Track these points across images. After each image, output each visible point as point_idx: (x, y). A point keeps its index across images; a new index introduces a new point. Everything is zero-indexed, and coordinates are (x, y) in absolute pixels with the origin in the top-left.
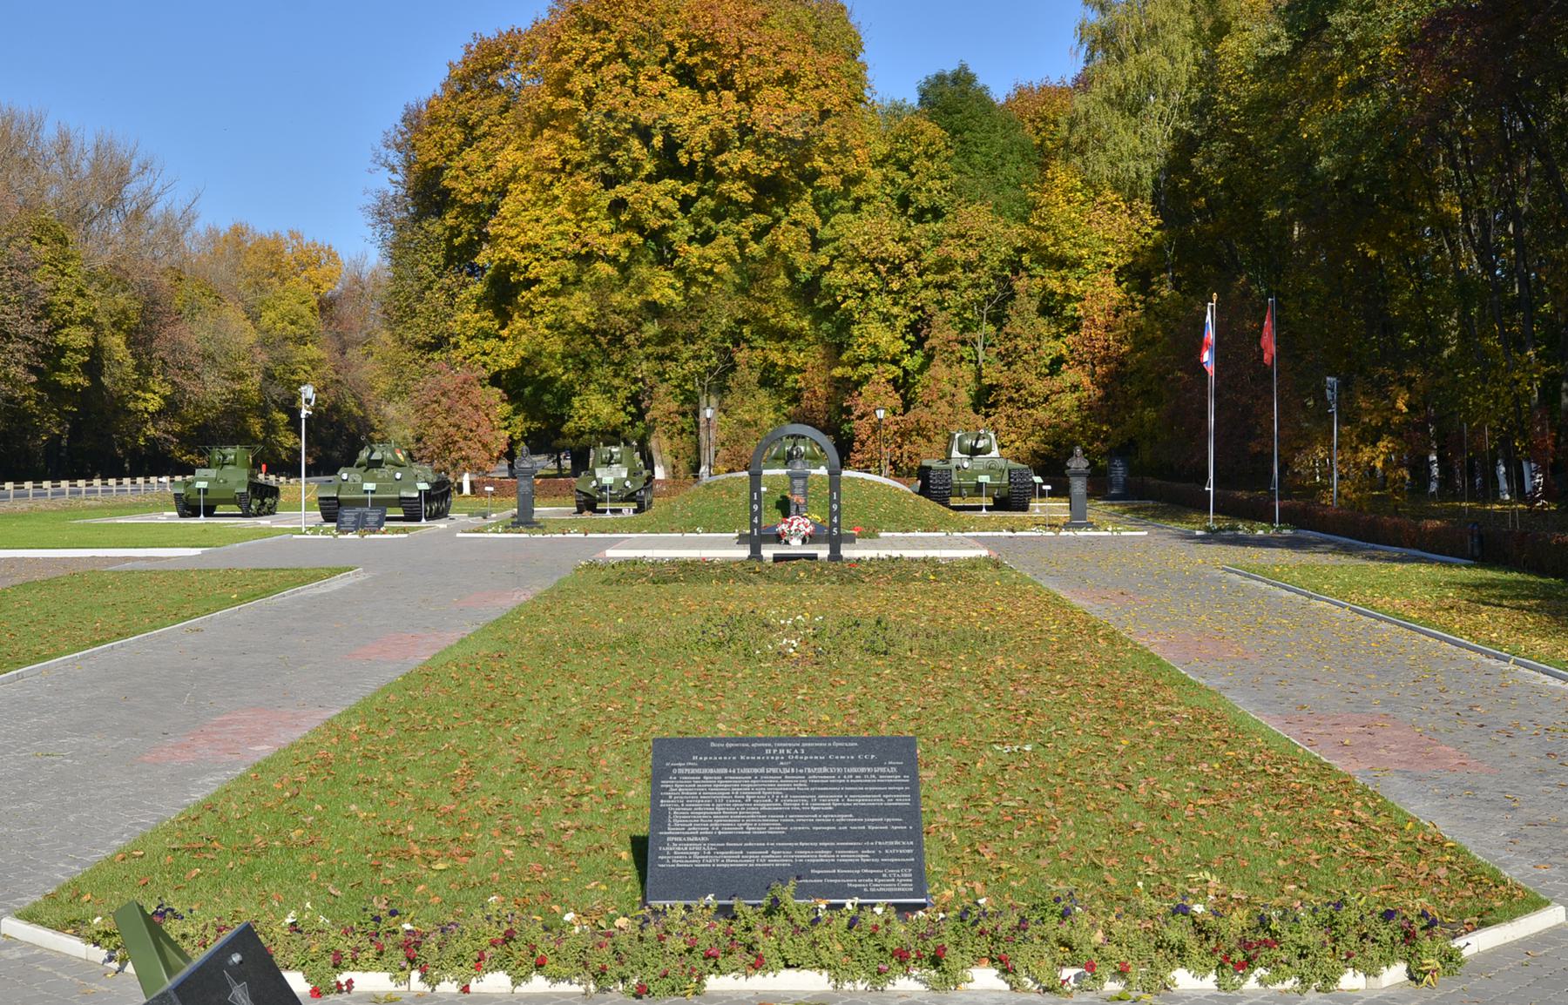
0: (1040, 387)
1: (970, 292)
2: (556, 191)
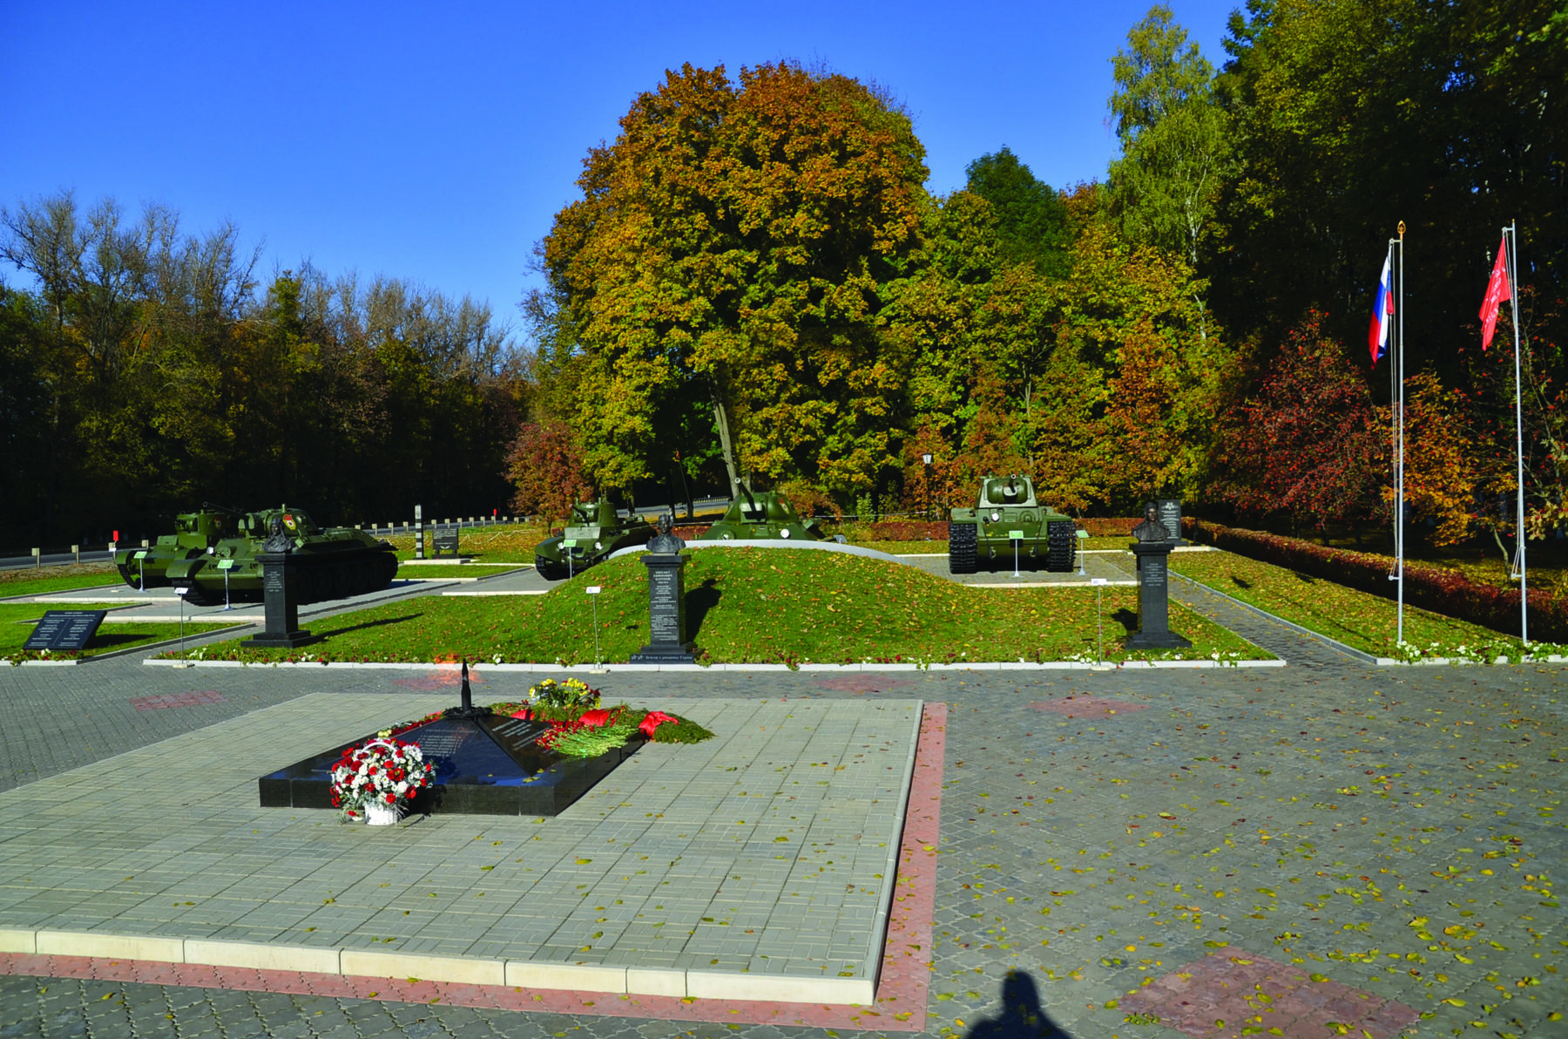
0: (1083, 429)
2: (638, 268)
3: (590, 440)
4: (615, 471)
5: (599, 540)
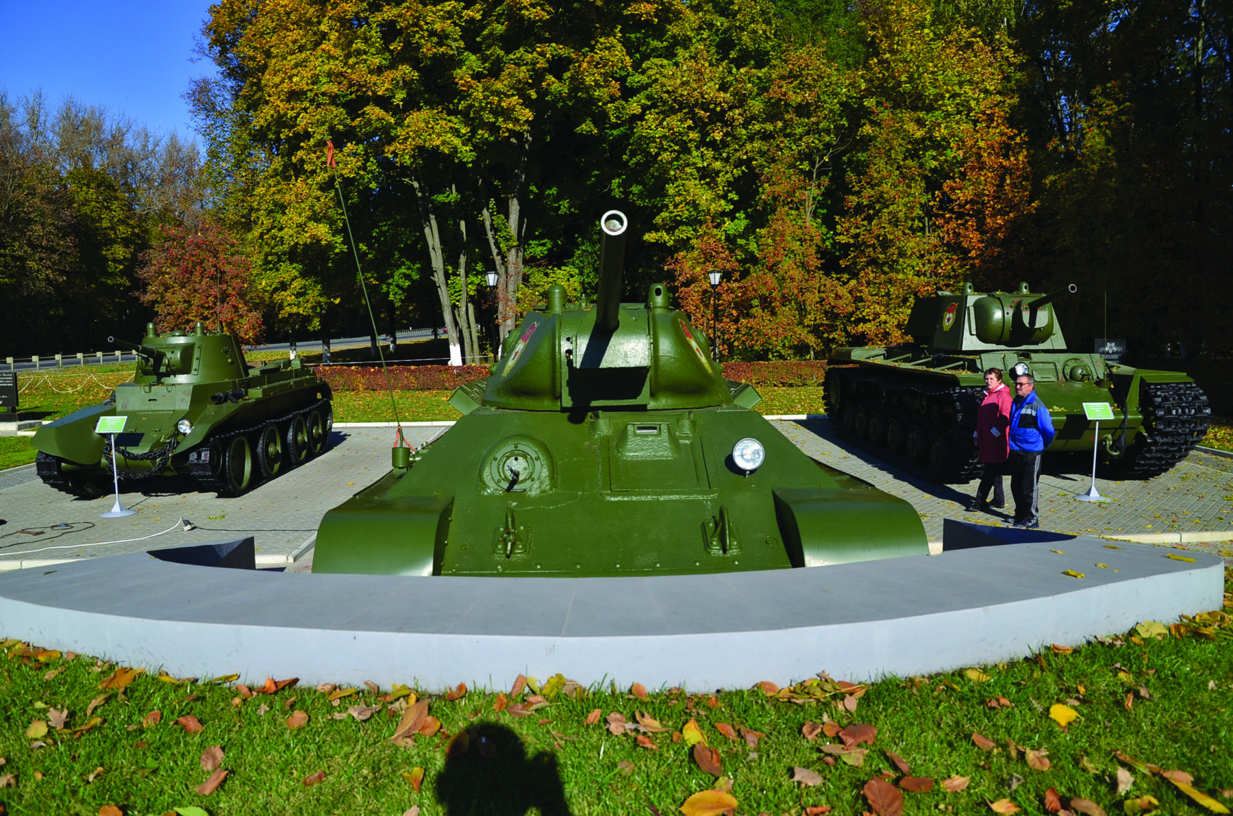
1: (810, 139)
2: (324, 28)
4: (298, 295)
5: (189, 416)
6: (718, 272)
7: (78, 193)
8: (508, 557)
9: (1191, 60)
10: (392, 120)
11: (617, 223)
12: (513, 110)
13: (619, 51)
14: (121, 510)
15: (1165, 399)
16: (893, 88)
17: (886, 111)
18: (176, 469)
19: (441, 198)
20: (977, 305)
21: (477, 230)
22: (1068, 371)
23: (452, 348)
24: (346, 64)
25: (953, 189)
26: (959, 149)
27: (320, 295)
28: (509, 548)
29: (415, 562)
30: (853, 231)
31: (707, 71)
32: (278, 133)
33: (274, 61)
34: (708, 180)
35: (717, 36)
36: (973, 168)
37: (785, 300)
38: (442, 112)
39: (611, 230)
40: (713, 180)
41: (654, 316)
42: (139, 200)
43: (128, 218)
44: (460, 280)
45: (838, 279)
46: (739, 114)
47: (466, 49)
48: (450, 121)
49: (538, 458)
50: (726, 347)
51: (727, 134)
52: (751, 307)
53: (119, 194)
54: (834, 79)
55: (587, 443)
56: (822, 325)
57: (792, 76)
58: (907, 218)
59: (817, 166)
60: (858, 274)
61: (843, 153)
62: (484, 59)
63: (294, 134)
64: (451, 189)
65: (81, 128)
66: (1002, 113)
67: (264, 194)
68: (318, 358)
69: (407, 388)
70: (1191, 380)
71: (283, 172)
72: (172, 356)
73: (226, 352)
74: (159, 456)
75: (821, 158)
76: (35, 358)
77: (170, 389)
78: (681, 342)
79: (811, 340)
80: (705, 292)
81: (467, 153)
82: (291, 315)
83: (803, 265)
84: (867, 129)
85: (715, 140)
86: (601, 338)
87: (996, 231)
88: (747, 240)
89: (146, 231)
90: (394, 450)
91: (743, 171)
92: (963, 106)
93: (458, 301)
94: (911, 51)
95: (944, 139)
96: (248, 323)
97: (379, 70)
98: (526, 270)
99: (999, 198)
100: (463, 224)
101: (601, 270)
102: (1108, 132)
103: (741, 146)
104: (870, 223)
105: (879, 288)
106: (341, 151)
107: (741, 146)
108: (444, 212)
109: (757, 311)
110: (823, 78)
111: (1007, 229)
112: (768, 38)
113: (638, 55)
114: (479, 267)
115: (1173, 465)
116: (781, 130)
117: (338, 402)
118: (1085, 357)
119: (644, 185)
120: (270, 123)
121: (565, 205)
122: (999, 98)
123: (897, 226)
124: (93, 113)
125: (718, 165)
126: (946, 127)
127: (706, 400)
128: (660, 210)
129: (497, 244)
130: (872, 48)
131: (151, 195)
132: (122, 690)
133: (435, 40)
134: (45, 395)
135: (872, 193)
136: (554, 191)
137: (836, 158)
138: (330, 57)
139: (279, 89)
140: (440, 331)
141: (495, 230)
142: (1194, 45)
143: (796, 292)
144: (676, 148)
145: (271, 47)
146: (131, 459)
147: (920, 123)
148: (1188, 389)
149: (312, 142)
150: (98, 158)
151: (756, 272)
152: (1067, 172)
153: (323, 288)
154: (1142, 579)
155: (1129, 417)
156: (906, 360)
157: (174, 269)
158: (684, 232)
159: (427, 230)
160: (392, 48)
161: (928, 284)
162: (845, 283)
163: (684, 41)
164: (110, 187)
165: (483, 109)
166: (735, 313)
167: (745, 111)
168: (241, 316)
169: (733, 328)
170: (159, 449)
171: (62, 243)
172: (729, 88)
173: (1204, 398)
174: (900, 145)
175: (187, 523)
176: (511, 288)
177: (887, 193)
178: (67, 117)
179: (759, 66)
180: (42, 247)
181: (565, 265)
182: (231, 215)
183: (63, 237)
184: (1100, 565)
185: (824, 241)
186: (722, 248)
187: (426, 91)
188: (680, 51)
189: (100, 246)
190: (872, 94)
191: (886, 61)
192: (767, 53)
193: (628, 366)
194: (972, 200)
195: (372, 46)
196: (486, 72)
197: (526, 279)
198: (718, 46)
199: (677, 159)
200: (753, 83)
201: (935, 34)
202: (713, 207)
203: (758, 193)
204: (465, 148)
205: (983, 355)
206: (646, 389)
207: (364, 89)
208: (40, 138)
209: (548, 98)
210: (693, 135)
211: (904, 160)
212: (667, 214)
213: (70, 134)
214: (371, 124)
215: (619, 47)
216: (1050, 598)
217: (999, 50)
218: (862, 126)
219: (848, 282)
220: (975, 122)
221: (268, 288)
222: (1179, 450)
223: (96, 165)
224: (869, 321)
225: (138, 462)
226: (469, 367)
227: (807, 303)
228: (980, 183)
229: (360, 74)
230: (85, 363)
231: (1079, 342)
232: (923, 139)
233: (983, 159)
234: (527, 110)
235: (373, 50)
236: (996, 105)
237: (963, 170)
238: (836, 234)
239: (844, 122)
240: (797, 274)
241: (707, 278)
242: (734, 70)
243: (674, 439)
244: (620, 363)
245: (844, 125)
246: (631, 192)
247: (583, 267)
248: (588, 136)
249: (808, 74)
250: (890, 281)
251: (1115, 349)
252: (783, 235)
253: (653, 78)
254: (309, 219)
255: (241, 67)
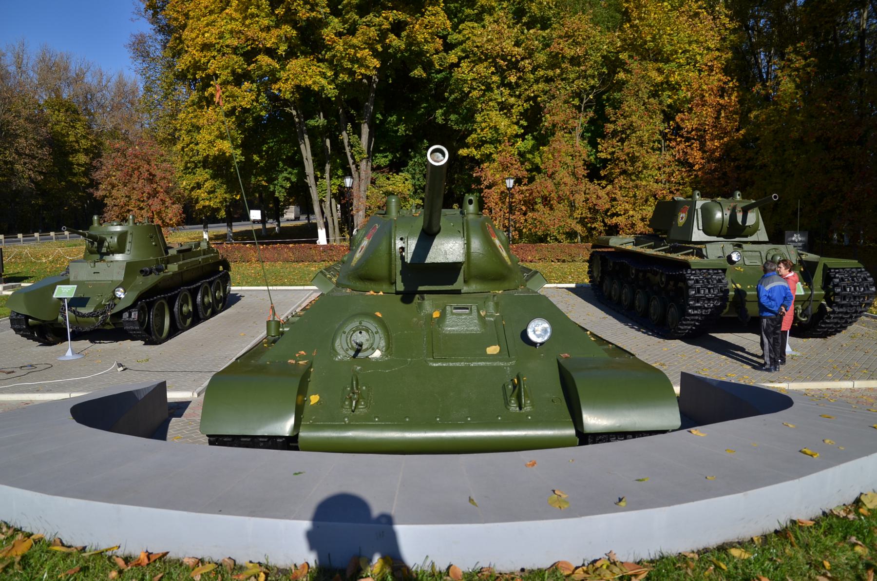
1: (580, 82)
3: (189, 165)
4: (209, 193)
5: (123, 285)
6: (512, 178)
7: (52, 116)
8: (353, 411)
9: (858, 27)
10: (277, 66)
11: (440, 155)
12: (365, 59)
13: (442, 17)
14: (73, 354)
15: (842, 280)
16: (641, 46)
17: (636, 63)
18: (114, 324)
19: (312, 122)
20: (703, 208)
21: (338, 146)
22: (769, 258)
23: (319, 231)
24: (243, 24)
25: (682, 120)
26: (688, 90)
27: (226, 193)
28: (354, 404)
29: (280, 416)
30: (610, 150)
31: (506, 32)
32: (194, 74)
33: (191, 21)
34: (505, 111)
35: (514, 6)
36: (697, 105)
37: (560, 199)
38: (313, 60)
39: (435, 161)
40: (509, 110)
41: (467, 221)
42: (96, 121)
43: (88, 134)
44: (326, 182)
45: (599, 184)
46: (529, 64)
47: (331, 14)
48: (319, 67)
49: (377, 333)
50: (517, 232)
51: (519, 78)
52: (536, 203)
53: (81, 117)
54: (598, 38)
55: (415, 319)
56: (586, 218)
57: (567, 36)
58: (649, 140)
59: (584, 102)
60: (613, 181)
61: (603, 93)
62: (344, 22)
63: (206, 75)
64: (319, 115)
65: (53, 69)
66: (720, 65)
67: (184, 118)
68: (223, 237)
69: (286, 260)
70: (861, 266)
71: (198, 102)
72: (111, 240)
73: (151, 237)
74: (101, 314)
75: (588, 96)
76: (20, 236)
77: (109, 265)
78: (488, 242)
79: (579, 228)
80: (502, 192)
81: (331, 91)
82: (204, 207)
83: (574, 174)
84: (622, 75)
85: (511, 82)
86: (427, 237)
87: (713, 151)
88: (533, 155)
89: (101, 144)
90: (268, 322)
91: (531, 105)
92: (691, 59)
93: (324, 197)
94: (655, 18)
95: (677, 83)
96: (173, 212)
97: (268, 29)
98: (374, 175)
99: (716, 127)
100: (328, 142)
101: (428, 176)
102: (797, 79)
103: (529, 87)
104: (622, 144)
105: (628, 191)
106: (240, 88)
107: (529, 87)
108: (314, 134)
109: (539, 206)
110: (589, 38)
111: (722, 149)
112: (550, 8)
113: (456, 20)
114: (340, 172)
115: (845, 328)
116: (559, 76)
117: (235, 271)
118: (782, 248)
119: (459, 114)
120: (189, 67)
121: (402, 128)
122: (717, 53)
123: (642, 146)
124: (62, 57)
125: (512, 100)
126: (679, 74)
127: (506, 285)
128: (470, 133)
129: (353, 156)
130: (626, 15)
131: (105, 118)
132: (18, 559)
133: (308, 7)
134: (26, 263)
135: (624, 122)
136: (394, 118)
137: (598, 97)
138: (232, 19)
139: (195, 42)
140: (311, 217)
141: (352, 146)
142: (860, 15)
143: (568, 193)
144: (483, 88)
145: (189, 11)
146: (80, 316)
147: (660, 71)
148: (858, 272)
149: (219, 81)
150: (66, 90)
151: (539, 178)
152: (767, 109)
153: (228, 188)
154: (865, 458)
155: (815, 292)
156: (649, 247)
157: (119, 173)
158: (488, 149)
159: (302, 146)
160: (277, 12)
161: (664, 189)
162: (604, 188)
163: (490, 10)
164: (75, 112)
165: (343, 58)
166: (524, 208)
167: (533, 61)
168: (167, 207)
169: (522, 219)
170: (101, 310)
171: (40, 152)
172: (521, 44)
173: (871, 279)
174: (646, 87)
175: (120, 365)
176: (362, 188)
177: (636, 122)
178: (43, 60)
179: (543, 28)
180: (26, 155)
181: (402, 171)
182: (161, 134)
183: (41, 148)
184: (827, 441)
185: (589, 156)
186: (516, 161)
187: (302, 45)
188: (487, 17)
189: (67, 154)
190: (625, 50)
191: (636, 26)
192: (549, 19)
193: (447, 261)
194: (696, 128)
195: (262, 11)
196: (345, 31)
197: (373, 182)
198: (514, 13)
199: (483, 95)
200: (539, 41)
201: (672, 6)
202: (509, 131)
203: (542, 121)
204: (330, 86)
205: (708, 245)
206: (461, 278)
207: (257, 43)
208: (24, 76)
209: (390, 51)
210: (495, 78)
211: (648, 98)
212: (476, 136)
213: (45, 72)
214: (262, 69)
215: (442, 13)
216: (797, 481)
217: (718, 18)
218: (618, 73)
219: (606, 187)
220: (700, 71)
221: (188, 187)
222: (851, 317)
223: (65, 96)
224: (621, 215)
225: (85, 319)
226: (332, 246)
227: (576, 202)
228: (702, 116)
229: (253, 31)
230: (56, 239)
231: (776, 237)
232: (662, 83)
233: (706, 98)
234: (375, 60)
235: (263, 14)
236: (715, 59)
237: (690, 106)
238: (597, 152)
239: (605, 70)
240: (569, 180)
241: (504, 182)
242: (526, 31)
243: (481, 319)
244: (441, 259)
245: (604, 72)
246: (450, 119)
247: (415, 174)
248: (419, 80)
249: (579, 35)
250: (637, 186)
251: (800, 239)
252: (559, 152)
253: (467, 36)
254: (217, 137)
255: (168, 26)
